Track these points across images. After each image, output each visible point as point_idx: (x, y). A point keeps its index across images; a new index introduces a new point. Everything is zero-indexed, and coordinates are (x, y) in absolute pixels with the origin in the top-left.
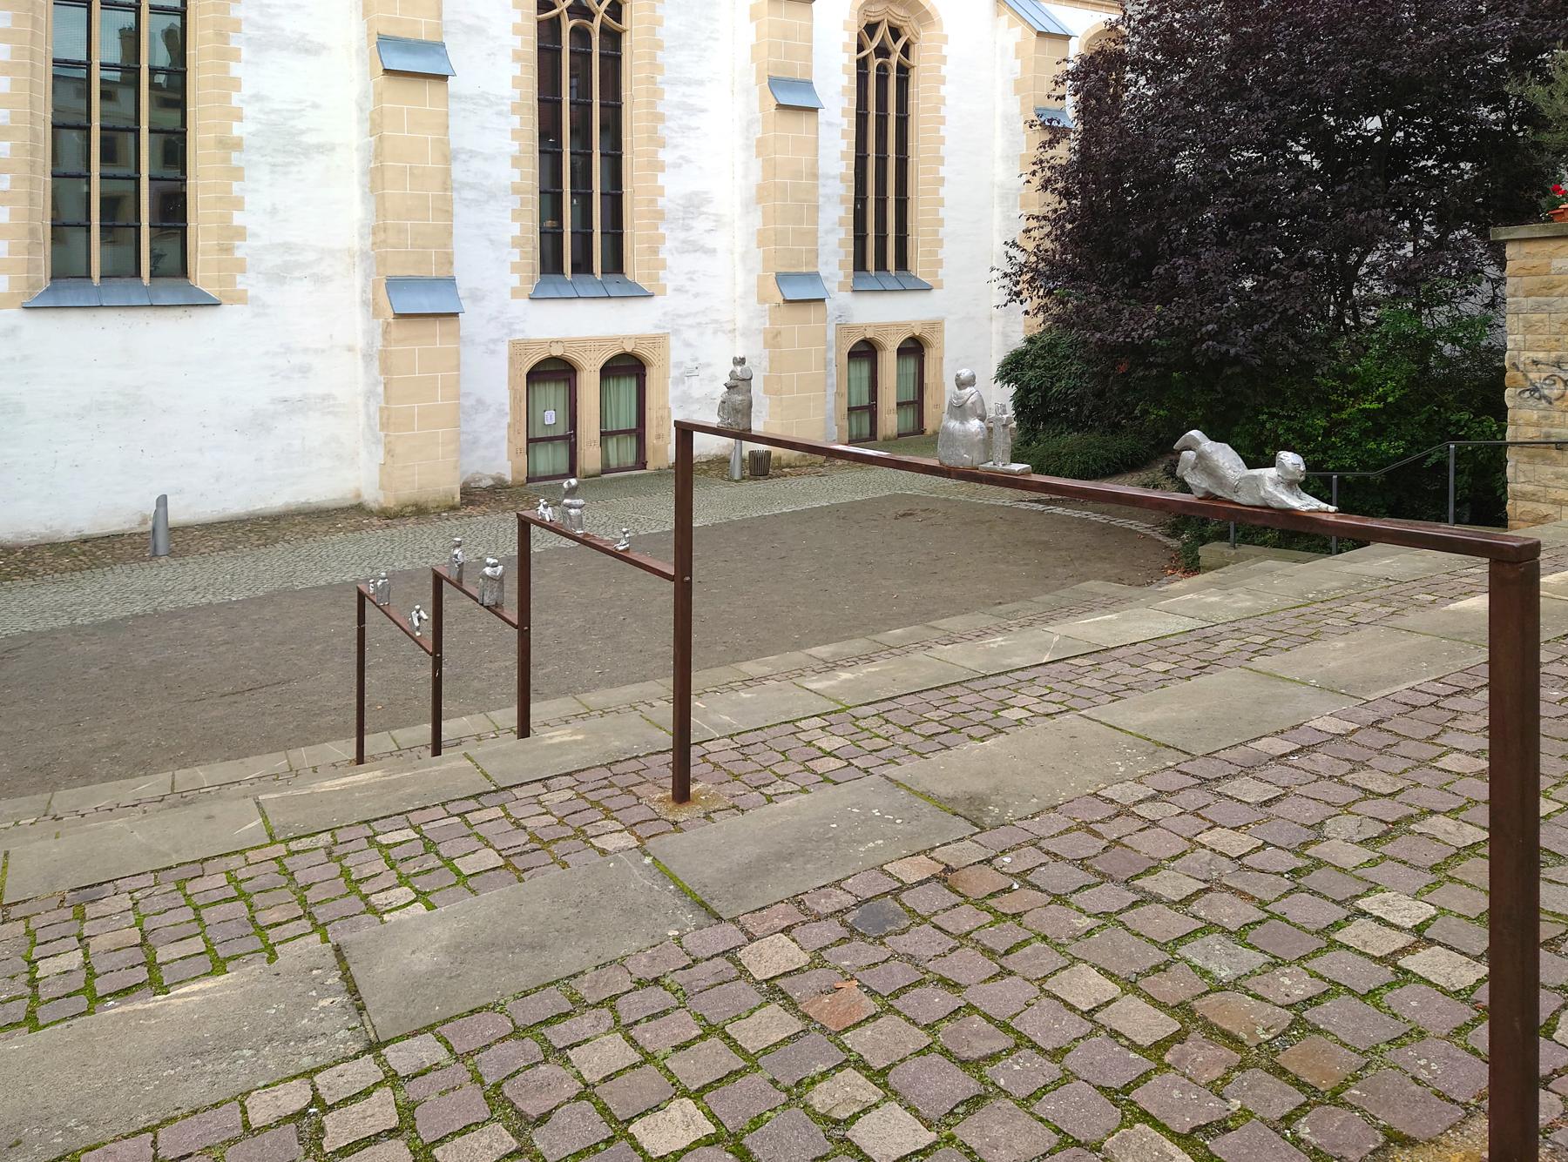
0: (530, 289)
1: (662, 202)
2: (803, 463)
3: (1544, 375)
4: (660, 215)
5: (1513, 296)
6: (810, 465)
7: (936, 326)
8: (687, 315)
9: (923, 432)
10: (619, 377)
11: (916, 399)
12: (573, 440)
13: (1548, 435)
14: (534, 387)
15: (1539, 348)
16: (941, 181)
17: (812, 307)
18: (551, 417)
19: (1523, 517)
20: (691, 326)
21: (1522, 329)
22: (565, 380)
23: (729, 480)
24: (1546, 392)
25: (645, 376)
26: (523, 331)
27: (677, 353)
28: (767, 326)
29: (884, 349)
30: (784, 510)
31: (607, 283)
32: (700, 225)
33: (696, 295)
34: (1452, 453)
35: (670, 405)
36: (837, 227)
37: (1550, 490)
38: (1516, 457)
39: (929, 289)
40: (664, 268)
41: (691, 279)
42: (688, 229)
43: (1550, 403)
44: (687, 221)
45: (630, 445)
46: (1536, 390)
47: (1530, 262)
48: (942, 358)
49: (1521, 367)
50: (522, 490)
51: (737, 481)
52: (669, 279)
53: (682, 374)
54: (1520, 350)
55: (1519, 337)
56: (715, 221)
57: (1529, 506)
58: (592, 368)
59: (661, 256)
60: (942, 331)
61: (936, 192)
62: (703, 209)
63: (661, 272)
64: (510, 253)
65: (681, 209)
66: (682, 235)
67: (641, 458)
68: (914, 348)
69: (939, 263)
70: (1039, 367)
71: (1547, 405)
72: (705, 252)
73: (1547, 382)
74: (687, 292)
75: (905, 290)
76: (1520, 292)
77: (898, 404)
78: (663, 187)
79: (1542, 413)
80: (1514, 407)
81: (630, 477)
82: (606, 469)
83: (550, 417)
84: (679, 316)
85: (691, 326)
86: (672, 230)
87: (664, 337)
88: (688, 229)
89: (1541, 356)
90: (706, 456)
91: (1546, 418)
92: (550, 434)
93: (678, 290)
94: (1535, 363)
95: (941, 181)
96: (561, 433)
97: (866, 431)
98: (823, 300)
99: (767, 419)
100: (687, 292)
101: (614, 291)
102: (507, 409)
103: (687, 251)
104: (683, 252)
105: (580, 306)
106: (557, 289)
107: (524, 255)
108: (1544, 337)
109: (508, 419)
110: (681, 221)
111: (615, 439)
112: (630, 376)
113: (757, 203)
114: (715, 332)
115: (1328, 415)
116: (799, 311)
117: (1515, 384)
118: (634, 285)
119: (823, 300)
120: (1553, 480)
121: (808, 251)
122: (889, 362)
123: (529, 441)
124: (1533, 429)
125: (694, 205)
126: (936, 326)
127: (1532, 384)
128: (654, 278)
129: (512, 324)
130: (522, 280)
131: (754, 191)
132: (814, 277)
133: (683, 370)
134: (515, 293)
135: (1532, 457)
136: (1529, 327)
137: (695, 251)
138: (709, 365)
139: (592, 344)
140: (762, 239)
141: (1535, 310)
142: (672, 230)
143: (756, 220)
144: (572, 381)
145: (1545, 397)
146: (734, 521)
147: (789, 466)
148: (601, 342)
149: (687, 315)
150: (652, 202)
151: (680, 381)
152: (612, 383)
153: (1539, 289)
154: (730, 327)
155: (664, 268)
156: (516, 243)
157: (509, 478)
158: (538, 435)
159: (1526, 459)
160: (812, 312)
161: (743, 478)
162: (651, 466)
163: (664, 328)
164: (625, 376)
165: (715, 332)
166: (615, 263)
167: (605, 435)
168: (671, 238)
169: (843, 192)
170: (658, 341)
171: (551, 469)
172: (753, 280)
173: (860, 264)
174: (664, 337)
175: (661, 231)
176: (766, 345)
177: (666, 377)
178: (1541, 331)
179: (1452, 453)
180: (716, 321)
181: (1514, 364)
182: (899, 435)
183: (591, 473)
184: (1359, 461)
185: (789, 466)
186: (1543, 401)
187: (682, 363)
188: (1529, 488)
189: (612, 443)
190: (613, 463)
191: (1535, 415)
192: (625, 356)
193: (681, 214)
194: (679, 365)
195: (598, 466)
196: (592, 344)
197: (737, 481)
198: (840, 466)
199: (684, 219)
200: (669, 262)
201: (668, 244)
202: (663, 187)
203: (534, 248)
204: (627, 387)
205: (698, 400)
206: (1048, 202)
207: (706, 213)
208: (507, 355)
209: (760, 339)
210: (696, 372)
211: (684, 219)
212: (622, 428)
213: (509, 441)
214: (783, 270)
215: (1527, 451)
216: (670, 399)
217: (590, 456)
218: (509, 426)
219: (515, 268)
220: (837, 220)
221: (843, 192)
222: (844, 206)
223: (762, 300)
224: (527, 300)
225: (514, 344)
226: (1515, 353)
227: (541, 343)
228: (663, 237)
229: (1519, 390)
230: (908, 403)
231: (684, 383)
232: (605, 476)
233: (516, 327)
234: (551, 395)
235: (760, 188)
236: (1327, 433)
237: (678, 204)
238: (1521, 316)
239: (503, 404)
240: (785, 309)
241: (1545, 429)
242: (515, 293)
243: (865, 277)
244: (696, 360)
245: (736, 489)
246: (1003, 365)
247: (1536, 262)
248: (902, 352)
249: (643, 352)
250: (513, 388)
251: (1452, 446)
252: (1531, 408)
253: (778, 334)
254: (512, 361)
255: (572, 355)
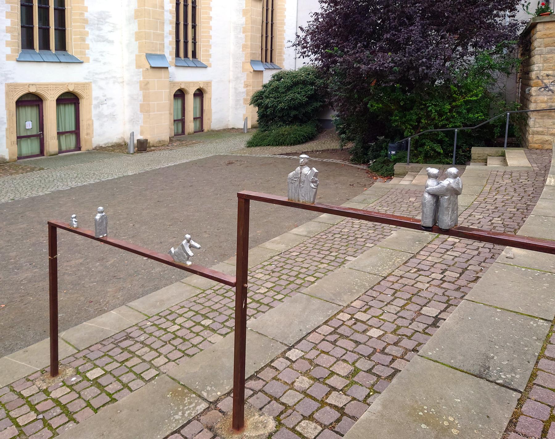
0: (17, 56)
1: (86, 15)
2: (159, 145)
3: (551, 81)
4: (86, 21)
5: (539, 47)
6: (162, 146)
7: (208, 83)
8: (100, 74)
9: (203, 131)
10: (65, 104)
11: (200, 116)
12: (42, 137)
13: (551, 106)
14: (19, 108)
15: (551, 69)
16: (210, 18)
17: (163, 70)
18: (30, 125)
19: (536, 142)
20: (102, 79)
21: (542, 61)
22: (36, 105)
23: (127, 153)
24: (552, 88)
25: (79, 103)
26: (13, 79)
27: (96, 92)
28: (142, 79)
29: (188, 93)
30: (170, 165)
31: (59, 55)
32: (106, 28)
33: (105, 64)
34: (508, 116)
35: (93, 118)
36: (168, 35)
37: (550, 129)
38: (535, 117)
39: (206, 67)
40: (88, 48)
41: (102, 55)
42: (100, 30)
43: (553, 93)
44: (99, 26)
45: (73, 138)
46: (547, 87)
47: (548, 32)
48: (211, 98)
49: (541, 78)
50: (16, 163)
51: (132, 154)
52: (91, 54)
53: (98, 103)
54: (540, 71)
55: (541, 65)
56: (113, 27)
57: (540, 137)
58: (52, 99)
59: (87, 42)
60: (211, 86)
61: (209, 23)
62: (107, 20)
63: (87, 51)
64: (5, 36)
65: (96, 19)
66: (97, 33)
67: (78, 145)
68: (200, 93)
69: (210, 56)
70: (272, 97)
71: (552, 93)
72: (109, 42)
73: (553, 83)
74: (100, 62)
75: (197, 67)
76: (543, 46)
77: (194, 119)
78: (87, 7)
79: (549, 97)
80: (536, 95)
81: (74, 154)
82: (60, 151)
83: (29, 125)
84: (96, 74)
85: (102, 79)
86: (92, 29)
87: (89, 84)
88: (100, 30)
89: (550, 72)
90: (111, 143)
91: (551, 99)
92: (29, 133)
93: (96, 60)
94: (548, 75)
95: (210, 18)
96: (35, 133)
97: (180, 131)
98: (167, 68)
99: (142, 125)
100: (100, 62)
101: (62, 59)
102: (5, 120)
103: (100, 41)
104: (98, 41)
105: (45, 66)
106: (32, 57)
107: (13, 36)
108: (552, 64)
109: (6, 126)
110: (96, 26)
111: (64, 136)
112: (71, 104)
113: (135, 19)
114: (114, 83)
115: (450, 104)
116: (157, 72)
117: (537, 85)
118: (72, 57)
119: (167, 68)
120: (551, 125)
121: (161, 44)
122: (190, 99)
123: (19, 138)
124: (544, 104)
125: (102, 18)
126: (208, 83)
127: (546, 85)
128: (84, 54)
129: (7, 74)
130: (13, 51)
131: (133, 13)
132: (163, 57)
133: (98, 101)
134: (8, 58)
135: (543, 116)
136: (545, 61)
137: (104, 41)
138: (111, 99)
139: (52, 86)
140: (138, 36)
141: (549, 53)
142: (92, 29)
143: (135, 27)
144: (40, 105)
145: (551, 90)
146: (148, 171)
147: (153, 146)
148: (56, 86)
149: (100, 74)
150: (82, 14)
151: (97, 106)
152: (62, 107)
153: (552, 44)
154: (121, 80)
155: (88, 48)
156: (9, 30)
157: (7, 157)
158: (22, 134)
159: (540, 117)
160: (163, 73)
161: (135, 153)
162: (84, 149)
163: (89, 79)
164: (68, 104)
165: (114, 83)
166: (62, 45)
167: (59, 134)
168: (92, 34)
169: (171, 19)
170: (86, 86)
171: (30, 152)
172: (133, 57)
173: (178, 55)
174: (89, 84)
175: (87, 29)
176: (141, 88)
177: (90, 104)
178: (551, 62)
179: (508, 116)
180: (115, 77)
181: (538, 77)
182: (195, 132)
183: (53, 153)
184: (462, 123)
185: (153, 146)
186: (550, 92)
187: (98, 97)
188: (541, 129)
189: (63, 138)
190: (64, 148)
191: (546, 98)
192: (69, 93)
193: (96, 22)
194: (97, 98)
195: (56, 149)
196: (52, 86)
197: (132, 154)
198: (176, 146)
199: (98, 24)
200: (91, 46)
201: (90, 37)
202: (87, 7)
203: (18, 34)
204: (70, 110)
205: (106, 116)
206: (242, 35)
207: (108, 23)
208: (4, 91)
209: (138, 86)
210: (105, 102)
211: (98, 24)
212: (68, 130)
213: (7, 138)
214: (149, 52)
215: (540, 114)
216: (93, 116)
217: (52, 144)
218: (7, 130)
219: (8, 44)
220: (168, 31)
221: (171, 19)
222: (171, 25)
223: (138, 67)
224: (15, 62)
225: (8, 85)
226: (538, 72)
227: (24, 85)
228: (88, 33)
229: (539, 88)
230: (178, 120)
231: (99, 107)
232: (60, 155)
233: (9, 76)
234: (30, 113)
235: (136, 11)
236: (451, 111)
237: (95, 17)
238: (542, 56)
239: (3, 118)
240: (151, 72)
241: (549, 104)
242: (8, 58)
243: (180, 60)
244: (105, 96)
245: (129, 158)
246: (254, 97)
247: (551, 32)
248: (195, 95)
249: (78, 91)
250: (8, 109)
251: (508, 114)
252: (544, 95)
253: (147, 83)
254: (7, 94)
255: (41, 92)
